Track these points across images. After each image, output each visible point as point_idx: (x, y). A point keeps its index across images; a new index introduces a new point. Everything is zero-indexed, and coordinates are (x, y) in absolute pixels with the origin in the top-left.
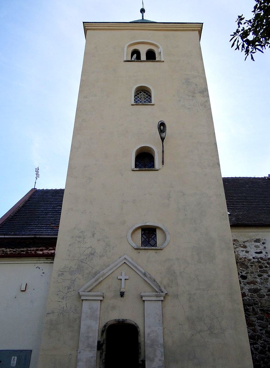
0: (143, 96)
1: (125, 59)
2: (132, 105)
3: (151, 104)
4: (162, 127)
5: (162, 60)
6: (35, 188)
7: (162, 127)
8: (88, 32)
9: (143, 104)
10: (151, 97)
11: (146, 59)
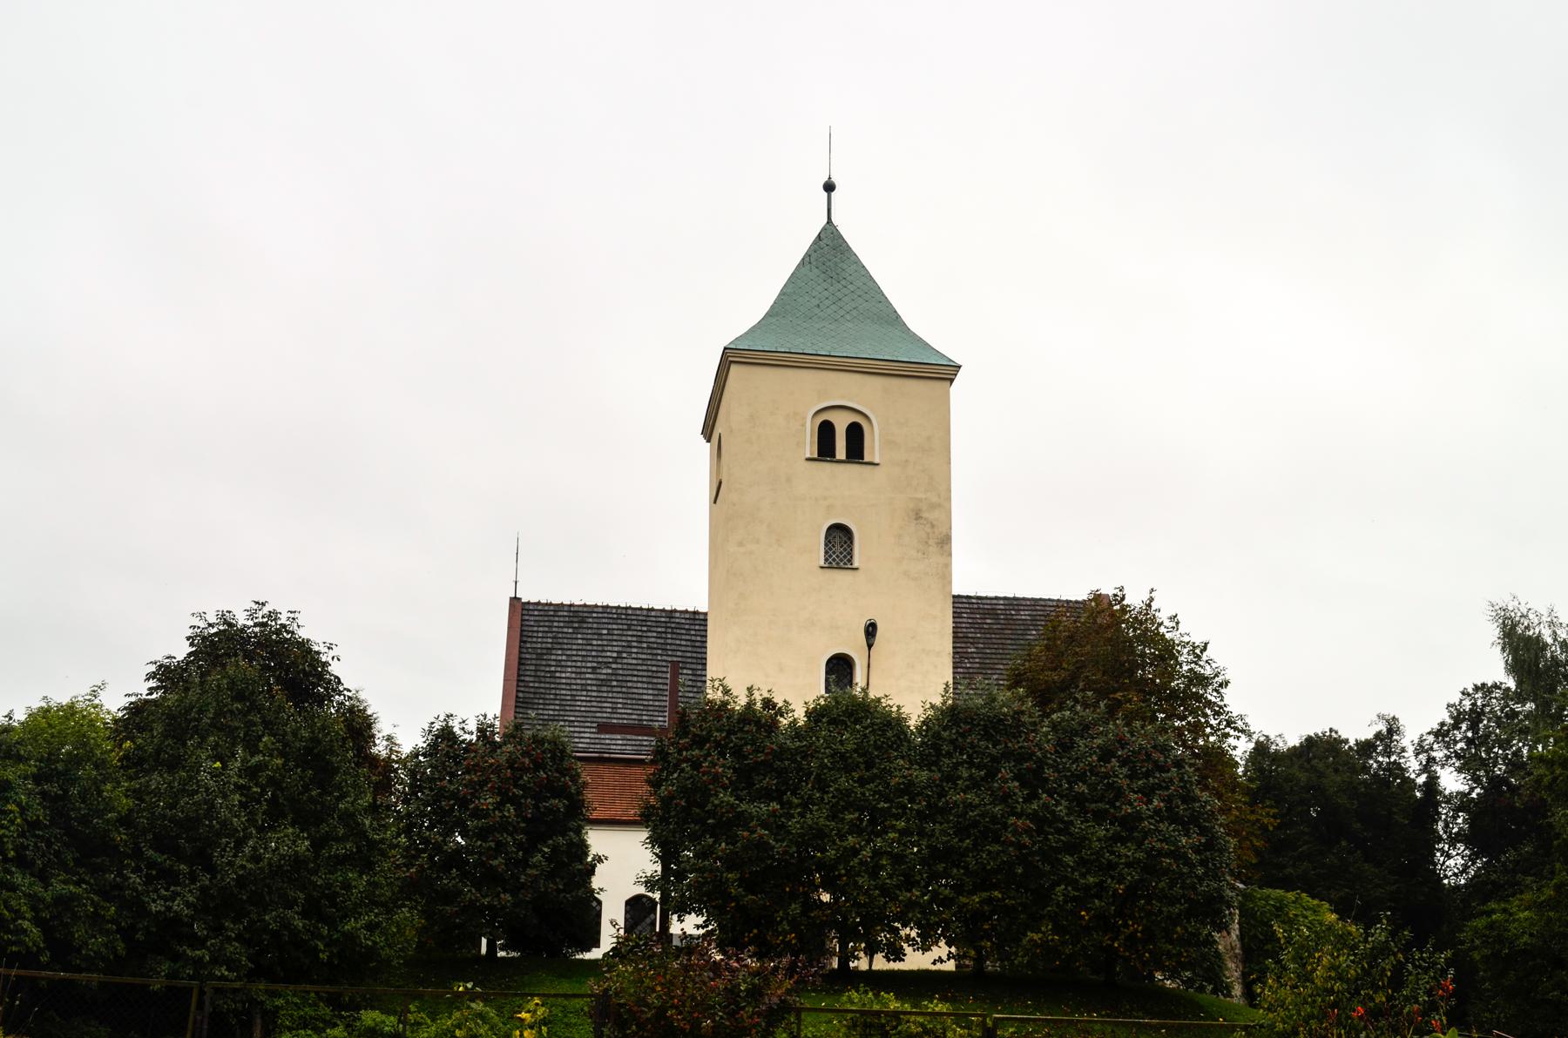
0: (837, 540)
1: (808, 455)
2: (822, 567)
3: (853, 566)
4: (871, 630)
5: (876, 461)
6: (517, 596)
7: (871, 629)
9: (830, 565)
10: (852, 542)
11: (847, 458)
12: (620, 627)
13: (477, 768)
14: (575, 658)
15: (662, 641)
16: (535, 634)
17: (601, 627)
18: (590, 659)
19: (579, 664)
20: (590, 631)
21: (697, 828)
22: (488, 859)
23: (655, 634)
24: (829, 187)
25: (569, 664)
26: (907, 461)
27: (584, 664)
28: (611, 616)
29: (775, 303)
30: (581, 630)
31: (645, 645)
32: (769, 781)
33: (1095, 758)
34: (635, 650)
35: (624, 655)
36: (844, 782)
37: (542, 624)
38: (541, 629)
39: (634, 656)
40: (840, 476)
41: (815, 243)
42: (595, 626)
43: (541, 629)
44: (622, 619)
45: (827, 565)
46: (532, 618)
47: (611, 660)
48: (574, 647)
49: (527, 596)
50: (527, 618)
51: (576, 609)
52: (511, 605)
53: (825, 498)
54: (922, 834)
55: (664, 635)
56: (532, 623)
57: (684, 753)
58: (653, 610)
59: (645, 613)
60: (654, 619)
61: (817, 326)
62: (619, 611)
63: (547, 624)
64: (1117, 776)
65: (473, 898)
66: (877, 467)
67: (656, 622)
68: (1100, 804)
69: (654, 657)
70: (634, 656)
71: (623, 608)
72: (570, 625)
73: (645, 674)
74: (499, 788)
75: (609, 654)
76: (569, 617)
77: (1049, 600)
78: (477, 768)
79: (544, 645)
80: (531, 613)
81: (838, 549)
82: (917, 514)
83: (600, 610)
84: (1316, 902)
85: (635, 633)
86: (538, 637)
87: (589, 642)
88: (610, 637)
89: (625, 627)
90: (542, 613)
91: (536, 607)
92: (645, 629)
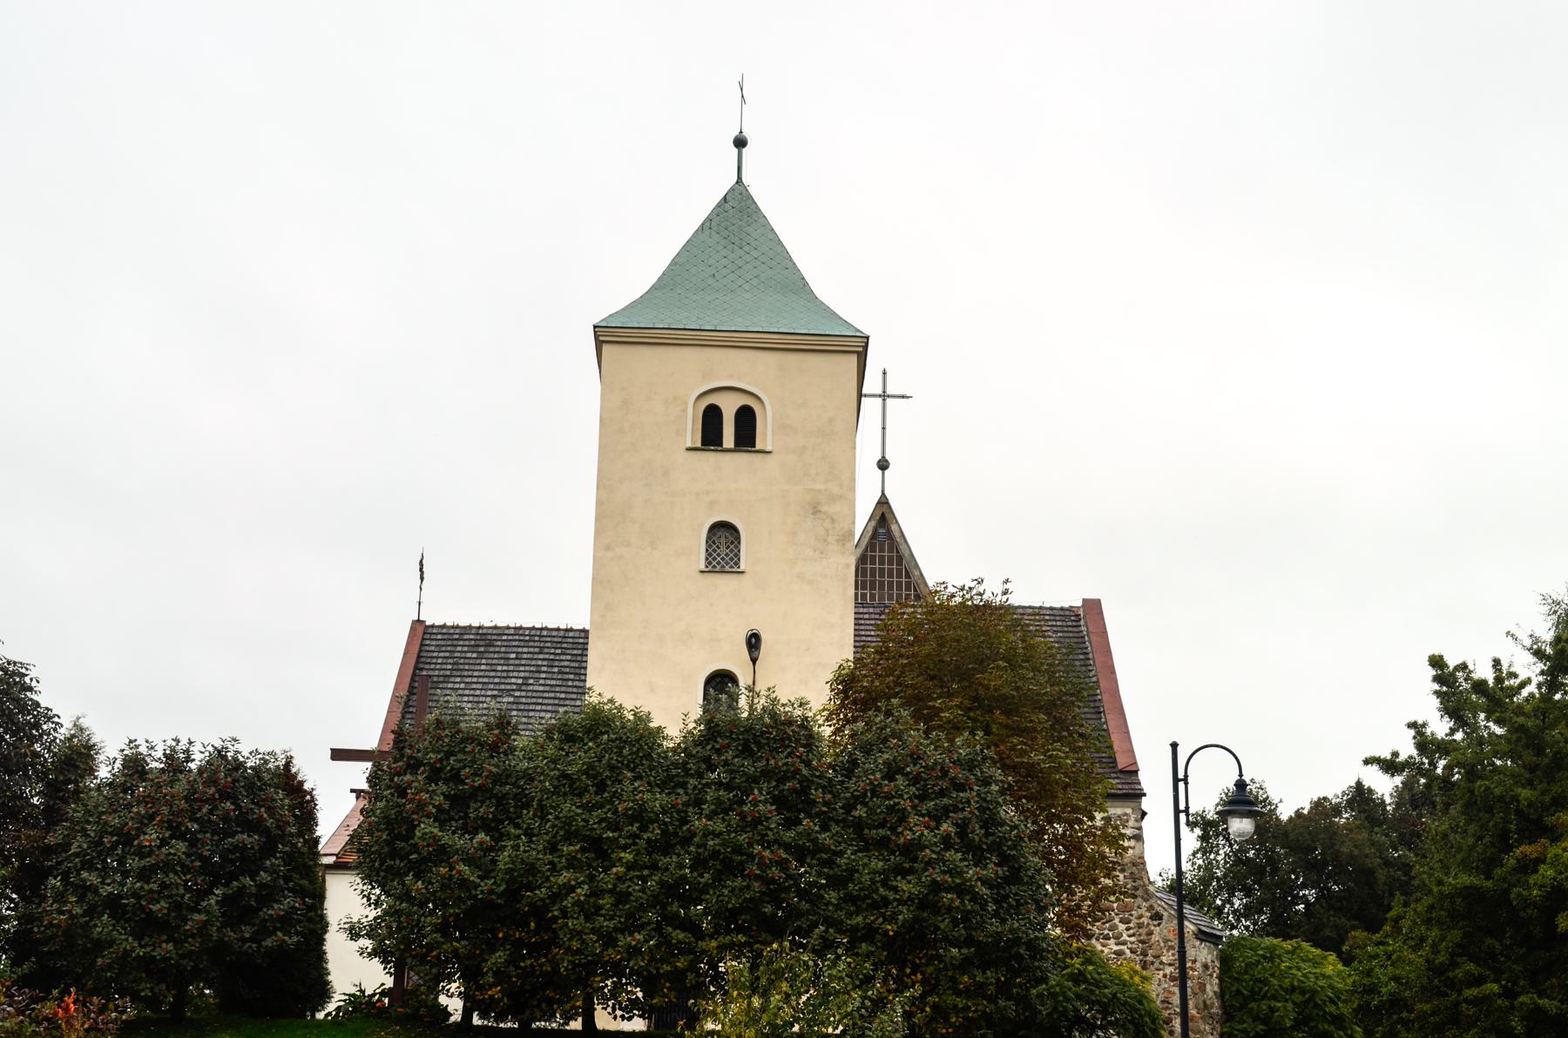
0: (723, 540)
1: (689, 445)
2: (702, 572)
3: (741, 570)
4: (754, 642)
5: (769, 448)
7: (753, 640)
8: (605, 348)
10: (739, 543)
12: (531, 650)
13: (148, 799)
14: (474, 686)
15: (576, 665)
16: (434, 661)
17: (510, 650)
18: (492, 686)
19: (478, 692)
20: (496, 656)
21: (402, 864)
22: (149, 903)
23: (569, 657)
24: (740, 143)
25: (467, 692)
26: (804, 447)
27: (483, 692)
28: (522, 638)
29: (664, 274)
30: (486, 655)
31: (556, 670)
32: (486, 810)
33: (878, 775)
34: (543, 675)
35: (531, 681)
36: (568, 807)
37: (443, 649)
38: (442, 654)
39: (542, 682)
40: (728, 465)
41: (718, 206)
42: (503, 649)
43: (442, 654)
44: (534, 641)
45: (710, 568)
46: (434, 643)
47: (514, 687)
48: (476, 674)
49: (431, 618)
50: (428, 642)
51: (485, 631)
52: (413, 629)
53: (707, 493)
54: (654, 867)
55: (579, 658)
56: (433, 648)
57: (396, 779)
58: (571, 630)
59: (562, 633)
60: (571, 640)
61: (708, 298)
62: (533, 633)
63: (449, 648)
64: (901, 796)
65: (128, 948)
66: (769, 456)
67: (573, 643)
68: (880, 831)
69: (564, 683)
70: (542, 682)
71: (538, 629)
72: (475, 649)
73: (551, 701)
74: (169, 822)
75: (513, 680)
76: (475, 640)
77: (1030, 607)
78: (148, 799)
79: (442, 673)
80: (433, 637)
81: (723, 551)
82: (815, 507)
83: (512, 631)
84: (1318, 951)
85: (547, 656)
86: (436, 664)
87: (494, 668)
88: (517, 662)
89: (537, 650)
90: (446, 637)
91: (440, 631)
92: (559, 651)
